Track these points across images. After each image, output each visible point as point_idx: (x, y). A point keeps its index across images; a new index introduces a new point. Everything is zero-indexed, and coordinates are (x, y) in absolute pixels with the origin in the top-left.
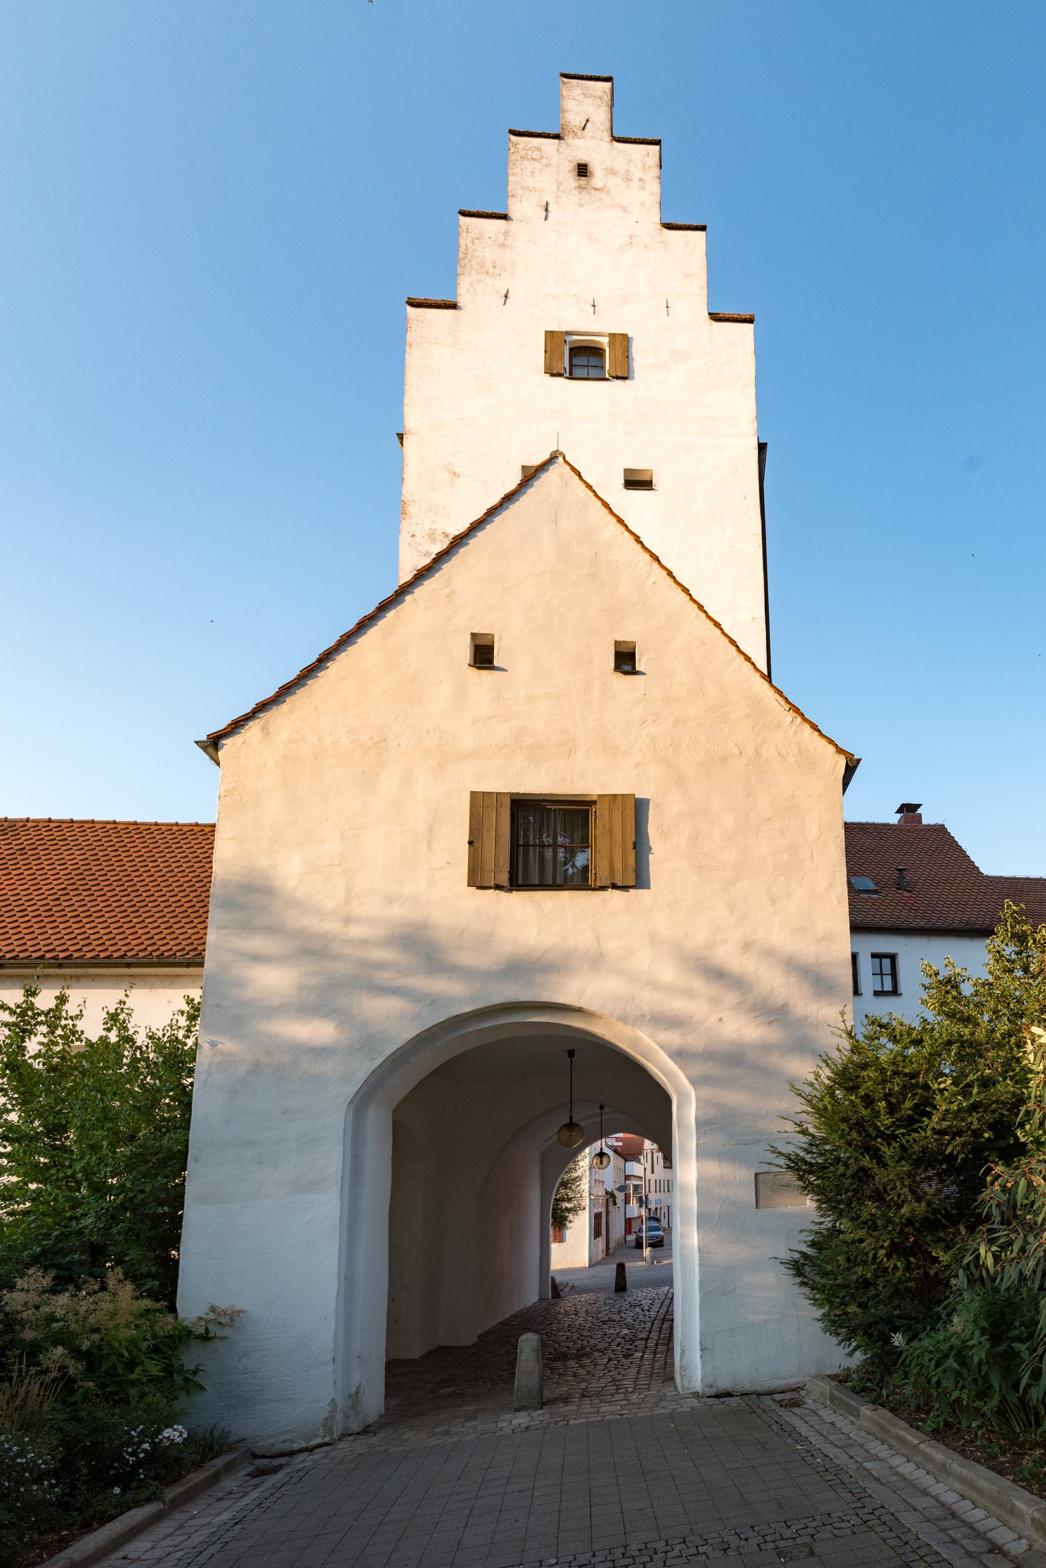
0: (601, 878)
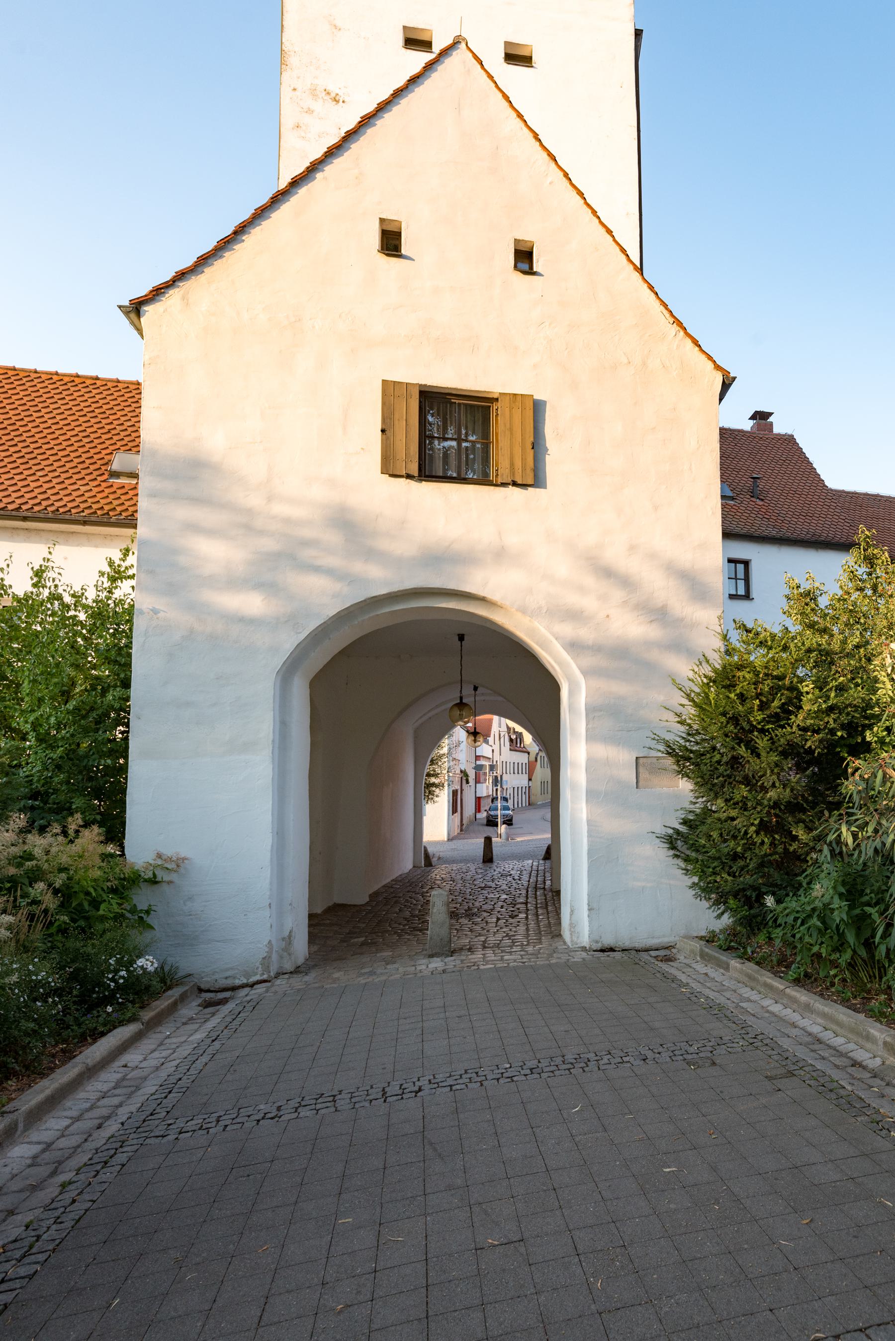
0: (502, 475)
